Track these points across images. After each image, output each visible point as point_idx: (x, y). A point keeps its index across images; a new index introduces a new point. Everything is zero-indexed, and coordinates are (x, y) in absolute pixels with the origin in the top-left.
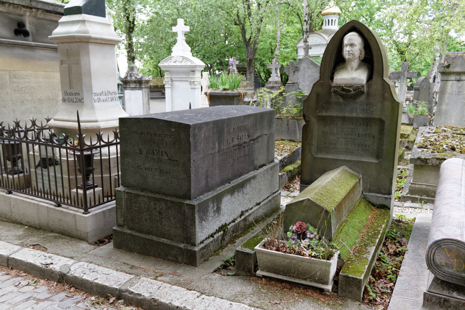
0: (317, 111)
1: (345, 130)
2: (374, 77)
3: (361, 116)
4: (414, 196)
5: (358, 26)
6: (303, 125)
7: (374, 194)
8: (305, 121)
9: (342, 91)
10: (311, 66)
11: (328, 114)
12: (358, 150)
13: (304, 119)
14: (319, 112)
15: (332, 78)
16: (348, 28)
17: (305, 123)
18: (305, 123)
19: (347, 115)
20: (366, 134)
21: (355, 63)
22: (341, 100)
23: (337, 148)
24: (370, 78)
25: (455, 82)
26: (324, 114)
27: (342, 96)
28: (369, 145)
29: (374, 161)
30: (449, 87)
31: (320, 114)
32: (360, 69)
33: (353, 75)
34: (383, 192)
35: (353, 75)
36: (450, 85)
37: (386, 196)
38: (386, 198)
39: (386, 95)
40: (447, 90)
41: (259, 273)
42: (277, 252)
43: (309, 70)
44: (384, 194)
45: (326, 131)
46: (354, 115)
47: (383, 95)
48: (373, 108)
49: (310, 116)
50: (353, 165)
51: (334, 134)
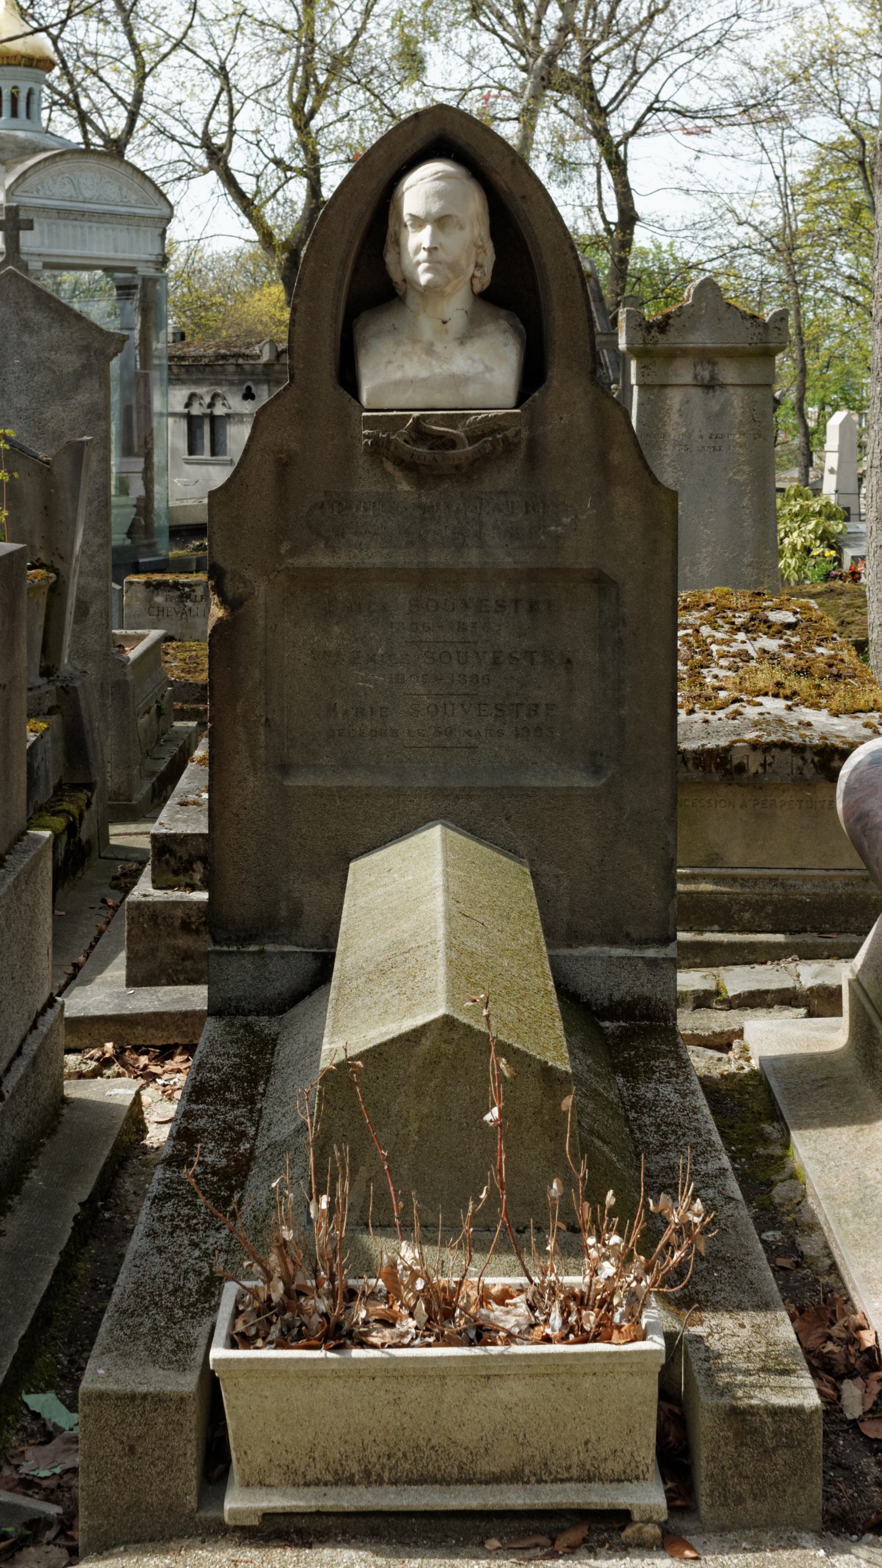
0: (285, 547)
1: (428, 636)
2: (556, 373)
3: (506, 561)
4: (708, 937)
5: (463, 137)
6: (211, 622)
7: (593, 949)
8: (224, 602)
9: (415, 442)
10: (37, 317)
11: (342, 559)
12: (500, 734)
13: (219, 589)
14: (291, 553)
15: (349, 380)
16: (416, 143)
17: (217, 612)
18: (217, 612)
19: (438, 558)
20: (529, 654)
21: (456, 306)
22: (404, 486)
23: (395, 733)
24: (532, 376)
25: (697, 394)
26: (322, 559)
27: (410, 467)
28: (550, 706)
29: (582, 781)
30: (675, 417)
31: (301, 561)
32: (479, 335)
33: (440, 365)
34: (635, 931)
35: (440, 365)
36: (676, 407)
37: (651, 953)
38: (652, 963)
39: (616, 457)
40: (669, 429)
41: (237, 1502)
42: (477, 1351)
43: (25, 338)
44: (643, 943)
45: (332, 646)
46: (473, 557)
47: (603, 456)
48: (558, 523)
49: (249, 574)
50: (479, 816)
51: (372, 659)
